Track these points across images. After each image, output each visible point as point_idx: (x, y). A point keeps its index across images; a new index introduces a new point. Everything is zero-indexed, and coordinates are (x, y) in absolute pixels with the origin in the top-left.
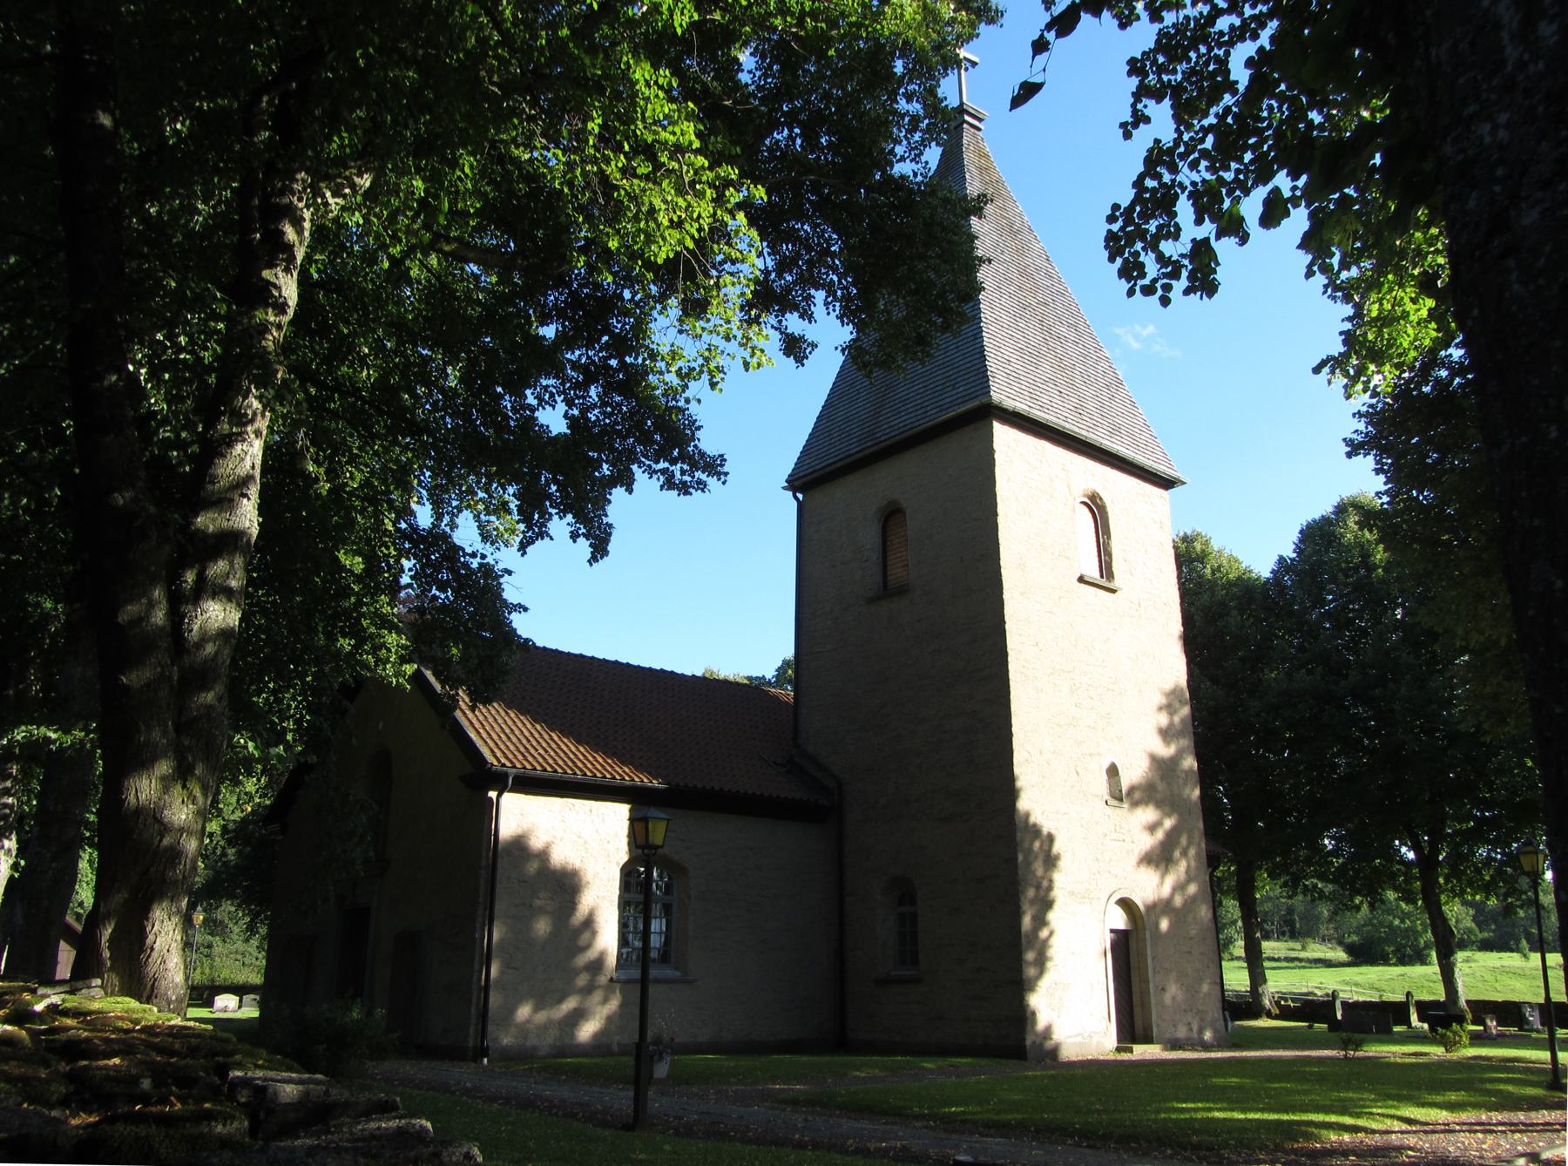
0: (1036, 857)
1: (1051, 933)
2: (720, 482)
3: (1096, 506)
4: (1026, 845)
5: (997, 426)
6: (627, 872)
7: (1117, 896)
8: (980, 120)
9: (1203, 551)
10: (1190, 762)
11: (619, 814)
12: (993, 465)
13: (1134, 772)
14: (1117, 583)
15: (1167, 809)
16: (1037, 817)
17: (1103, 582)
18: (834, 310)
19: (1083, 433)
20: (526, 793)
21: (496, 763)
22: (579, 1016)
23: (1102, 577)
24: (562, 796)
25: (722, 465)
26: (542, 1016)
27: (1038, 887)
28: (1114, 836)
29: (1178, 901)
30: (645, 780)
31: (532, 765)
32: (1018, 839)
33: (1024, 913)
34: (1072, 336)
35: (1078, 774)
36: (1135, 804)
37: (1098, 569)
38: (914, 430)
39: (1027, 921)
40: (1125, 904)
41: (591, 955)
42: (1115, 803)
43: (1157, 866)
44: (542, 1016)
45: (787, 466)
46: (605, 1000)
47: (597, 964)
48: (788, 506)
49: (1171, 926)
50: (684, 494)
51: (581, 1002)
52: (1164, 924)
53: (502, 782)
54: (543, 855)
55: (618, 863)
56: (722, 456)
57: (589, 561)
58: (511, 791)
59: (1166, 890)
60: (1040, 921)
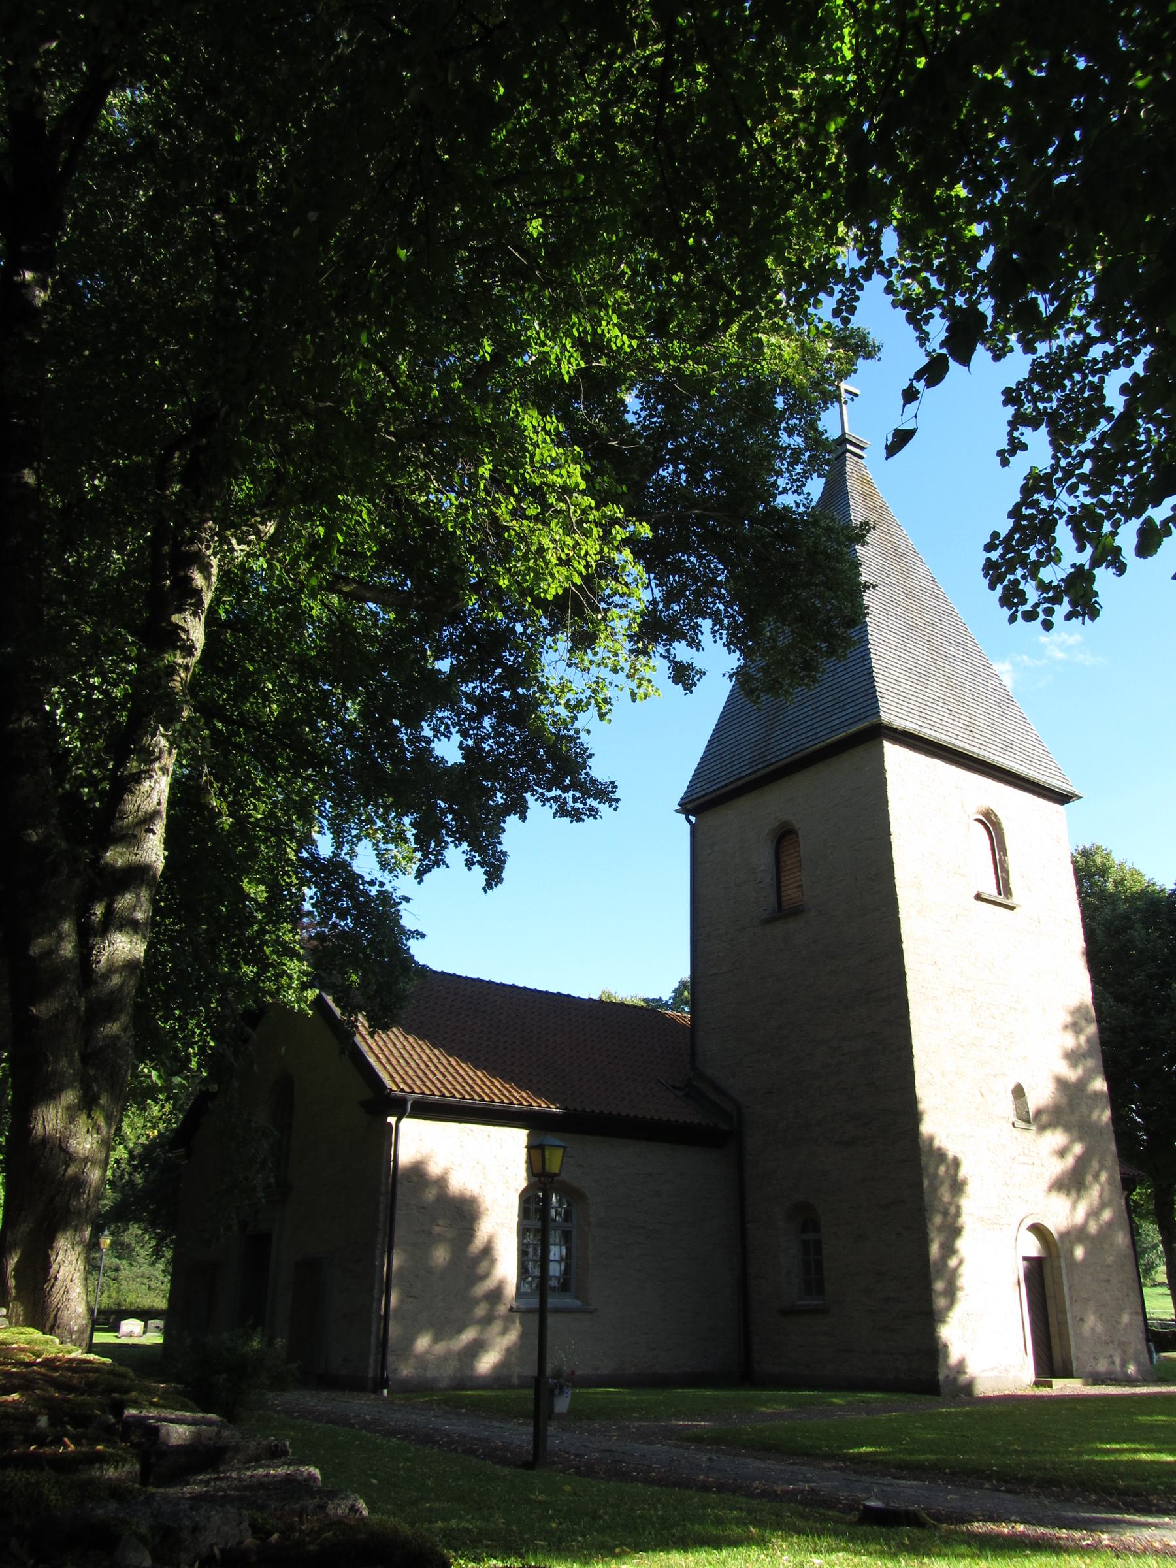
0: (942, 1183)
1: (961, 1262)
3: (991, 823)
4: (931, 1170)
8: (862, 448)
9: (1104, 864)
10: (1100, 1085)
11: (516, 1138)
12: (885, 785)
13: (1041, 1095)
16: (937, 1143)
17: (1001, 899)
18: (721, 638)
19: (975, 750)
20: (425, 1119)
21: (394, 1088)
22: (477, 1348)
23: (999, 893)
24: (460, 1122)
27: (945, 1213)
29: (1093, 1228)
32: (923, 1163)
33: (932, 1241)
34: (960, 655)
35: (982, 1095)
36: (1042, 1128)
37: (995, 886)
38: (805, 752)
39: (935, 1249)
41: (490, 1284)
42: (1023, 1124)
43: (1068, 1194)
44: (440, 1348)
45: (680, 789)
46: (505, 1331)
47: (496, 1294)
48: (680, 829)
49: (1086, 1253)
52: (1079, 1252)
53: (400, 1106)
54: (441, 1182)
57: (484, 888)
59: (1079, 1216)
60: (949, 1249)
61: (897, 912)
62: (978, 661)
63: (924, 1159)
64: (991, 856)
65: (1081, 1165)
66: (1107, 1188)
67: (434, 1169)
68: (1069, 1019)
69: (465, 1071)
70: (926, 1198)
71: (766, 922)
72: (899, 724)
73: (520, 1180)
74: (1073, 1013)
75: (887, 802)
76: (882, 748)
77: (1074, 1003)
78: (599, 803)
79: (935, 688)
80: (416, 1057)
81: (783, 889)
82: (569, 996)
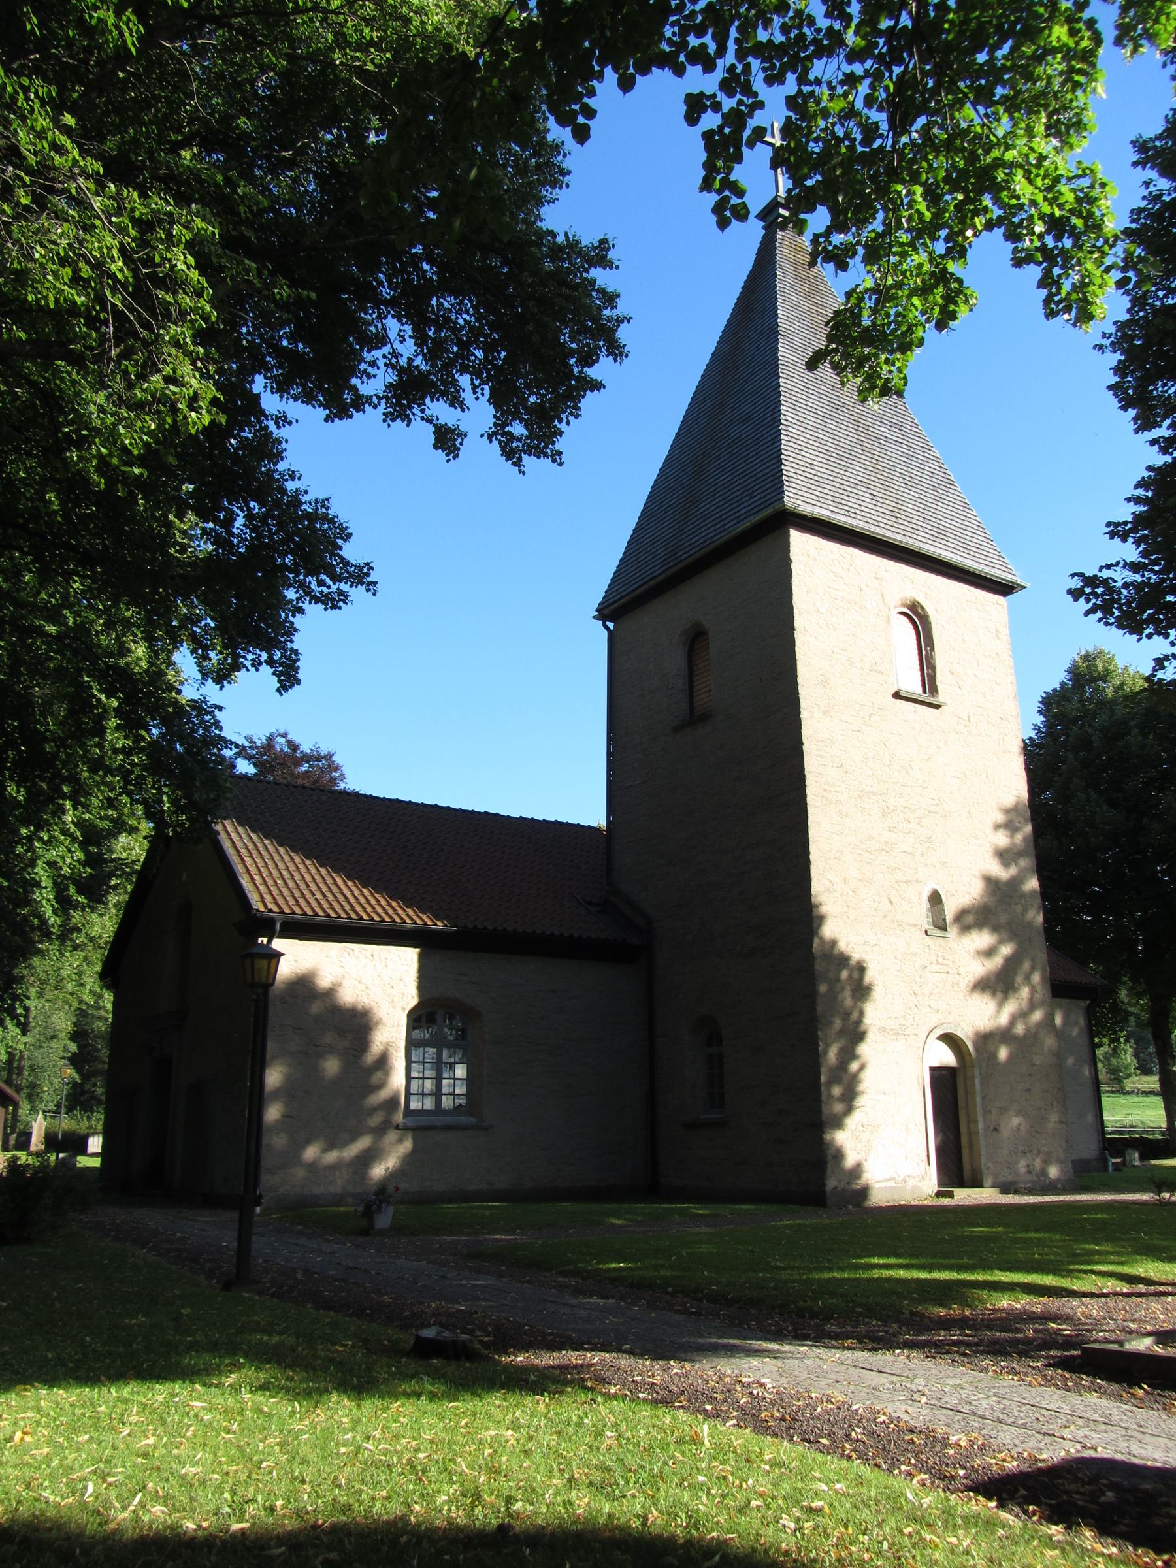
0: (843, 989)
2: (370, 593)
3: (917, 616)
5: (796, 537)
6: (417, 1018)
7: (939, 1032)
9: (1106, 669)
10: (1033, 884)
12: (790, 576)
14: (941, 698)
15: (1005, 935)
16: (843, 946)
18: (483, 394)
19: (898, 537)
21: (262, 908)
23: (924, 691)
25: (368, 575)
26: (332, 1156)
28: (935, 967)
29: (1020, 1029)
30: (429, 923)
31: (313, 910)
33: (828, 1045)
34: (894, 435)
35: (891, 902)
36: (965, 929)
37: (920, 683)
38: (713, 545)
40: (950, 1039)
41: (384, 1094)
42: (939, 933)
43: (994, 994)
44: (332, 1156)
46: (400, 1141)
48: (598, 636)
49: (1011, 1057)
50: (332, 608)
51: (375, 1142)
52: (1003, 1053)
53: (268, 925)
54: (330, 993)
55: (404, 1009)
56: (367, 564)
57: (278, 690)
58: (280, 937)
59: (1004, 1019)
60: (849, 1054)
61: (799, 712)
62: (916, 442)
63: (819, 966)
64: (916, 652)
65: (1010, 965)
66: (1039, 988)
67: (324, 981)
68: (1000, 818)
69: (350, 890)
70: (819, 1009)
71: (676, 729)
72: (806, 509)
73: (411, 998)
74: (1007, 812)
75: (791, 594)
76: (788, 536)
77: (1009, 801)
78: (351, 586)
79: (857, 471)
80: (297, 877)
81: (695, 694)
82: (497, 815)
